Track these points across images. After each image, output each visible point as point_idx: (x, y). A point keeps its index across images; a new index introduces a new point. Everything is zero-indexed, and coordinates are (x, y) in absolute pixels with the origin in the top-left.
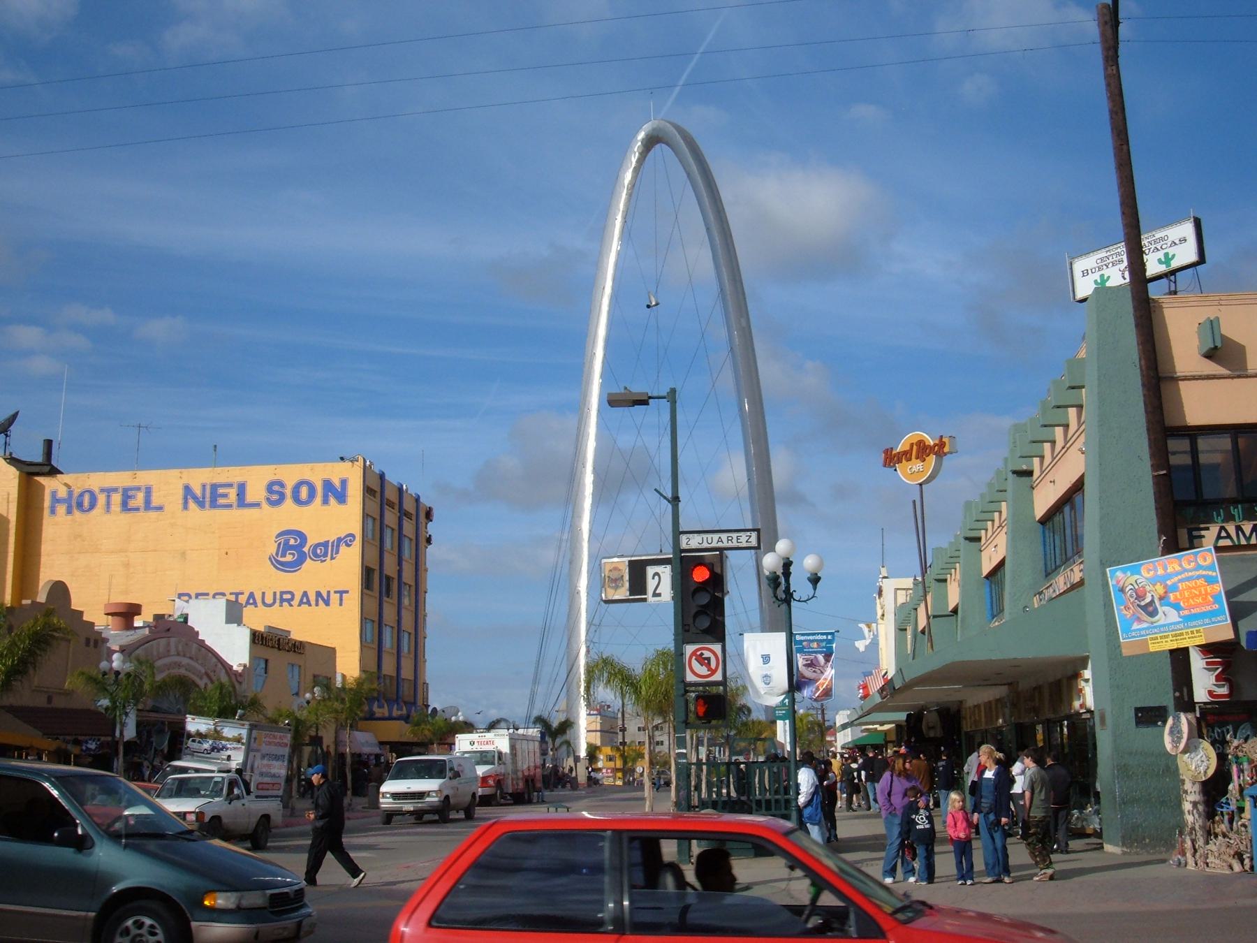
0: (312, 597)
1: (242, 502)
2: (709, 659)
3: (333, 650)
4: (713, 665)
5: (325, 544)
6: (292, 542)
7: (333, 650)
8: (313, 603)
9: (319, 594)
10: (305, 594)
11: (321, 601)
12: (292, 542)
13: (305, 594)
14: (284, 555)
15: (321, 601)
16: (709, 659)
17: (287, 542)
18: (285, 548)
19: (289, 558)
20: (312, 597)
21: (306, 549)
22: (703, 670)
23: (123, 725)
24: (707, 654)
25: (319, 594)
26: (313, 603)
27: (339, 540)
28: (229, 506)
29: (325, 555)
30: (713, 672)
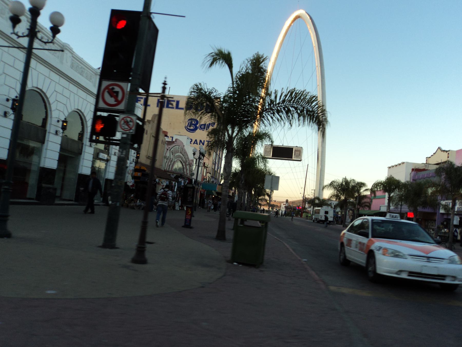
0: (198, 142)
1: (177, 107)
2: (117, 93)
3: (278, 178)
4: (120, 98)
5: (205, 125)
6: (193, 123)
7: (278, 178)
8: (198, 143)
9: (201, 141)
10: (196, 140)
11: (201, 143)
12: (193, 123)
13: (196, 140)
14: (190, 127)
15: (201, 143)
16: (117, 93)
17: (191, 122)
18: (191, 125)
19: (192, 128)
20: (198, 142)
21: (198, 126)
22: (111, 101)
23: (453, 220)
24: (117, 89)
25: (201, 141)
26: (198, 143)
27: (210, 124)
28: (173, 108)
29: (204, 128)
30: (119, 103)
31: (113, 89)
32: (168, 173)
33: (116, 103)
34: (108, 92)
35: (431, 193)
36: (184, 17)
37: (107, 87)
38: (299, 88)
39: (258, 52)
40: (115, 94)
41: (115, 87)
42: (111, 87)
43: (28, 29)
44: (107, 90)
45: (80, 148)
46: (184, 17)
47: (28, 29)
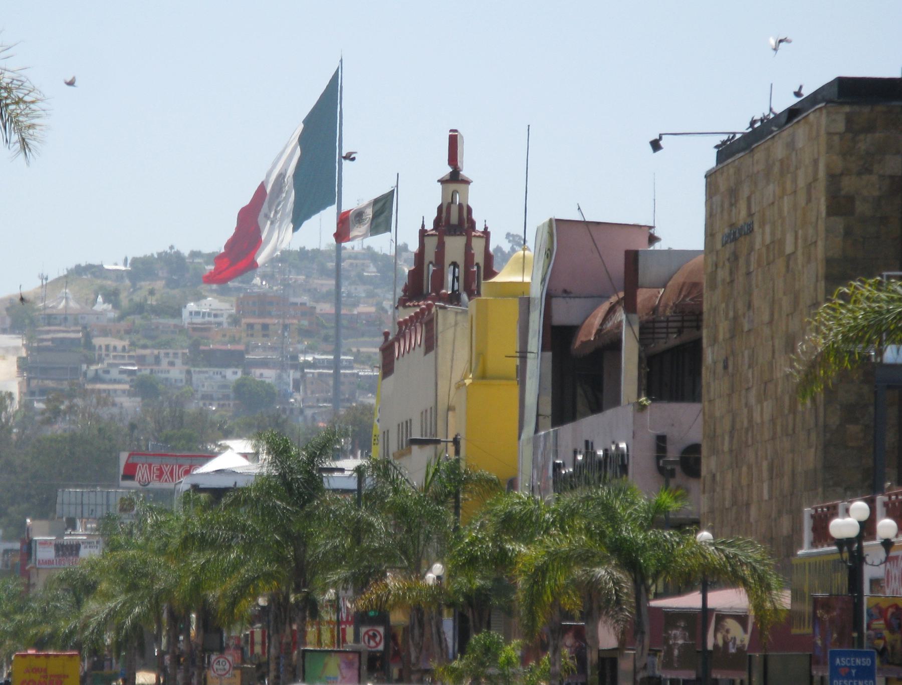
36: (454, 141)
46: (454, 141)
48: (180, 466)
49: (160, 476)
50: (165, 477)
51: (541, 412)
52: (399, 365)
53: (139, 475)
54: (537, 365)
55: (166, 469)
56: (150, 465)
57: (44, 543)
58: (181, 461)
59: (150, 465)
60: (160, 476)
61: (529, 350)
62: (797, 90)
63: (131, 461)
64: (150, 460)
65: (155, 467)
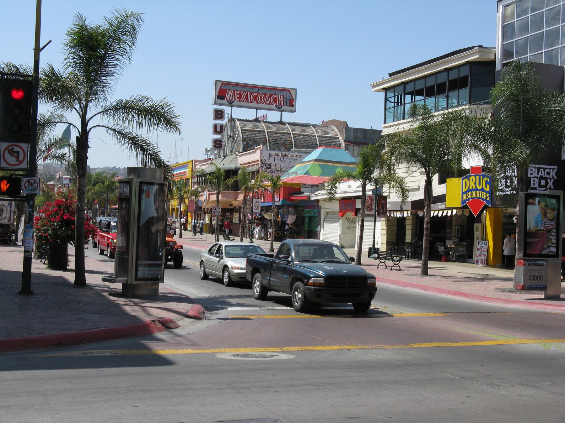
2: (18, 153)
4: (21, 158)
16: (18, 153)
30: (21, 162)
31: (13, 149)
32: (71, 250)
33: (18, 163)
34: (8, 152)
35: (424, 152)
36: (50, 41)
37: (7, 148)
38: (67, 39)
39: (80, 17)
40: (16, 154)
41: (14, 147)
42: (10, 148)
43: (89, 147)
44: (7, 151)
45: (138, 292)
46: (50, 41)
47: (89, 147)
48: (252, 93)
49: (240, 98)
50: (242, 99)
51: (461, 68)
52: (155, 96)
53: (227, 97)
54: (275, 418)
55: (244, 94)
56: (234, 91)
57: (66, 178)
58: (252, 90)
59: (234, 91)
60: (240, 98)
61: (283, 113)
62: (97, 20)
63: (223, 88)
64: (235, 88)
65: (237, 93)
